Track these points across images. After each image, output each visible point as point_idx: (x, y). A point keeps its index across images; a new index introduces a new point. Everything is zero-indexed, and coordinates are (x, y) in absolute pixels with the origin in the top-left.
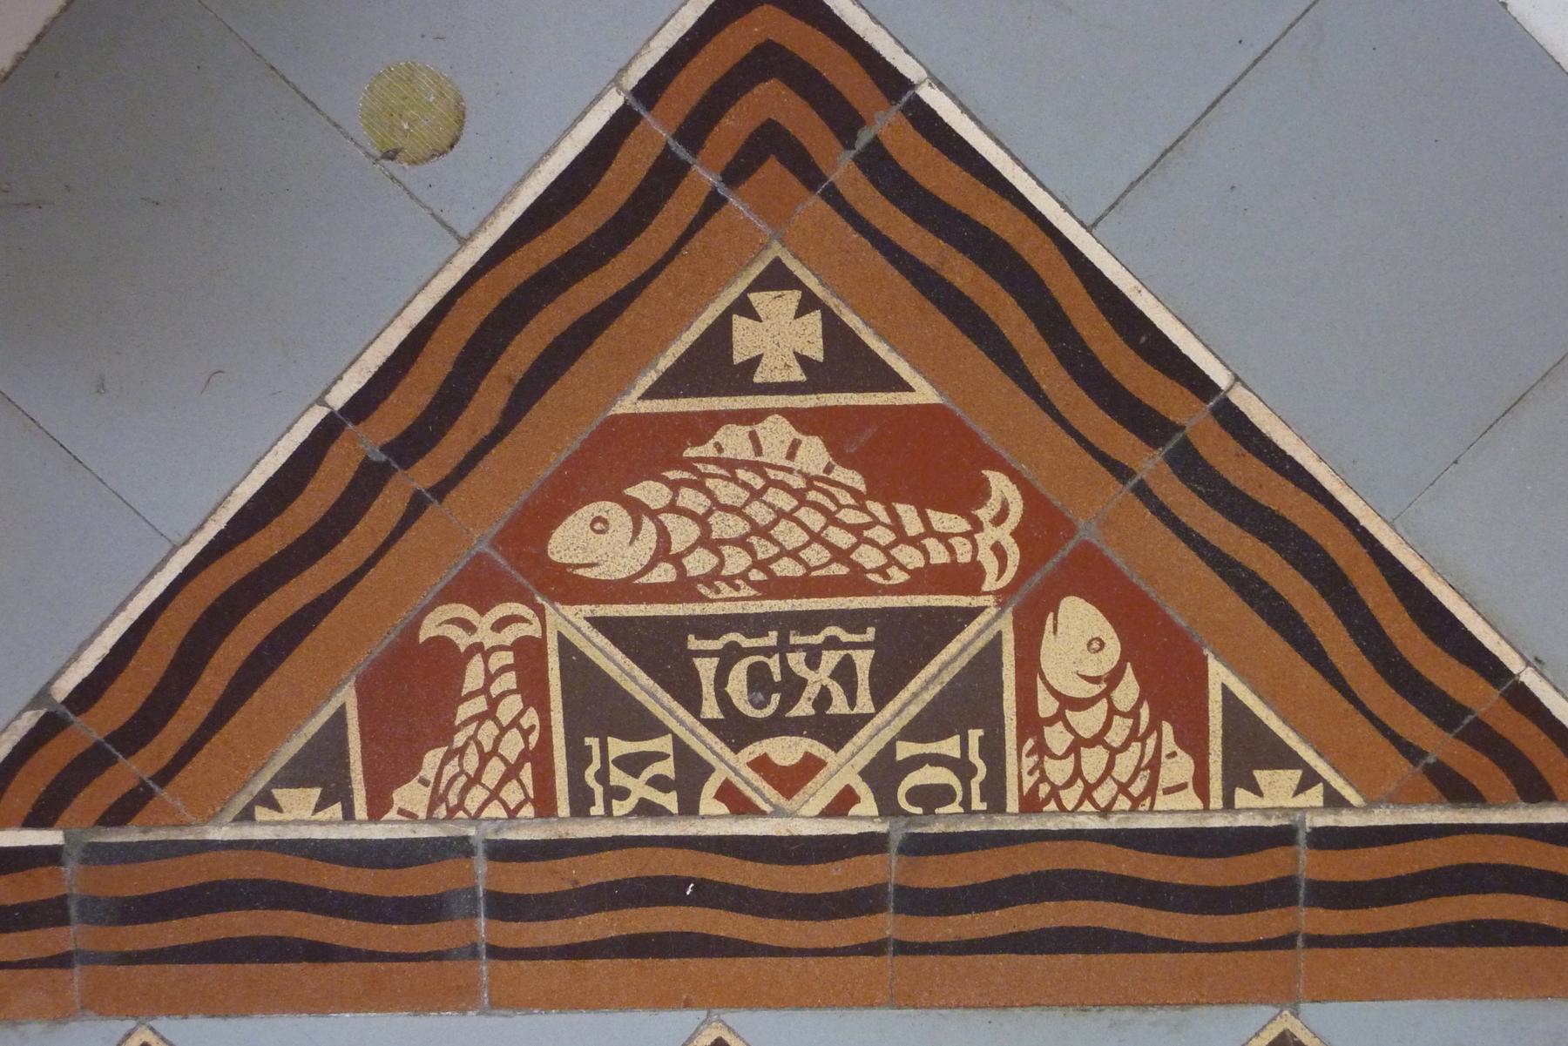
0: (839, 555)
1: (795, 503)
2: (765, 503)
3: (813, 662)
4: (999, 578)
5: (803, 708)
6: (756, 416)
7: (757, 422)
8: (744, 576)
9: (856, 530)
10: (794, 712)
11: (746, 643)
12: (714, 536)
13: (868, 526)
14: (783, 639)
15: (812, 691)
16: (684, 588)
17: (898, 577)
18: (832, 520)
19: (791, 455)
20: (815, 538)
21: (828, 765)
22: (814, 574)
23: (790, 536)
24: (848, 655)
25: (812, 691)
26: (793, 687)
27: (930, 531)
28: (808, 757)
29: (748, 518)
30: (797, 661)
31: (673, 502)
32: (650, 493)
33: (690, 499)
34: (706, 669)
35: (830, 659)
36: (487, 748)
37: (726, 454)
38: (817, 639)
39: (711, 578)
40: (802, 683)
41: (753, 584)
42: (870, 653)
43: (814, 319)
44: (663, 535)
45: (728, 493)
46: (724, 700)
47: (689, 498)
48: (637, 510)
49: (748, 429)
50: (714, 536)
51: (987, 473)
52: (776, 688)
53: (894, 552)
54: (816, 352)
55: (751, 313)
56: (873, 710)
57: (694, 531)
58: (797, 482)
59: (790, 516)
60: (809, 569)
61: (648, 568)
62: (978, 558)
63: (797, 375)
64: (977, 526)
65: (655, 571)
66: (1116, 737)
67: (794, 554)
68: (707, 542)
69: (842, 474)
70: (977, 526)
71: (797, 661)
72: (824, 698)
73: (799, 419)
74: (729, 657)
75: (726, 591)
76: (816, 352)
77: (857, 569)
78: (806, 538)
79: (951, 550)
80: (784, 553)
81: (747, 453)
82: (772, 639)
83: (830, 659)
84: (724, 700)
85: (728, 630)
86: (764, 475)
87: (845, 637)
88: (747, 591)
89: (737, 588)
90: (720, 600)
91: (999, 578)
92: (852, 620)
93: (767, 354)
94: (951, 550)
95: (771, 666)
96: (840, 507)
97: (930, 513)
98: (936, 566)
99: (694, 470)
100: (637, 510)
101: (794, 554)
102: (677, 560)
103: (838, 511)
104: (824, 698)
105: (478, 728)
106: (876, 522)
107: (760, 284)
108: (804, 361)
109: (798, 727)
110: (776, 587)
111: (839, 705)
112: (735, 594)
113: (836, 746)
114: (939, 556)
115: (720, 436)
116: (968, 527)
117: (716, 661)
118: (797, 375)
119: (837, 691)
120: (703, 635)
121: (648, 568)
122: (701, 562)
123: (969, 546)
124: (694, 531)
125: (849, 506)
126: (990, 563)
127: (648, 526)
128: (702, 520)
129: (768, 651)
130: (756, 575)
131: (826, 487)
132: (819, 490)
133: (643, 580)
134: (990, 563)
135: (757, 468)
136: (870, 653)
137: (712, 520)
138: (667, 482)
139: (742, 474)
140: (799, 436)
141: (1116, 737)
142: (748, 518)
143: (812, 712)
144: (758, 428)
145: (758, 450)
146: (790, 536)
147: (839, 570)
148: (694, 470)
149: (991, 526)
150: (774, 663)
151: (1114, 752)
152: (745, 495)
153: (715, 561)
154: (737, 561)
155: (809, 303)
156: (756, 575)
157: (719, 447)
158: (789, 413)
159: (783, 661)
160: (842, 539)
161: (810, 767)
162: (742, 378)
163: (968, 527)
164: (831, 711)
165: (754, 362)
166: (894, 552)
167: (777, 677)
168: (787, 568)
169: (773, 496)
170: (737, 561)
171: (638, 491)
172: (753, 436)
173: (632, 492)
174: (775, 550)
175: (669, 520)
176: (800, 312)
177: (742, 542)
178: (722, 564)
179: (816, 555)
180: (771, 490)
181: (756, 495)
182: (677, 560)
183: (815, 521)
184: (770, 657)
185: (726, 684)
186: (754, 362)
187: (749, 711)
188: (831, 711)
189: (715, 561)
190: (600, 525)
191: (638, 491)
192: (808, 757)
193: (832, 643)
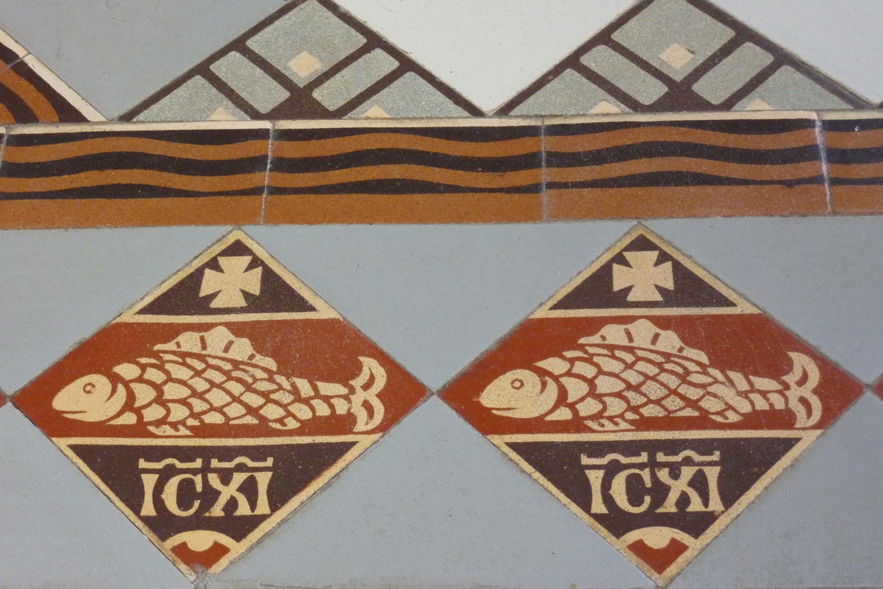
0: (251, 411)
1: (225, 378)
2: (635, 370)
3: (675, 474)
4: (367, 424)
5: (217, 511)
6: (208, 327)
7: (630, 323)
8: (621, 416)
9: (265, 395)
10: (660, 510)
11: (179, 465)
12: (598, 392)
13: (274, 391)
14: (652, 457)
15: (222, 501)
16: (577, 424)
17: (292, 424)
18: (249, 388)
19: (226, 350)
20: (236, 399)
21: (231, 551)
22: (232, 422)
23: (218, 398)
24: (252, 475)
25: (222, 501)
26: (211, 494)
27: (753, 389)
28: (673, 541)
29: (190, 387)
30: (214, 480)
31: (570, 370)
32: (127, 370)
33: (155, 375)
34: (595, 478)
35: (688, 472)
36: (711, 389)
37: (609, 341)
38: (678, 458)
39: (159, 423)
40: (668, 489)
41: (191, 428)
42: (717, 469)
43: (668, 265)
44: (131, 397)
45: (182, 373)
46: (608, 500)
47: (581, 368)
48: (115, 379)
49: (624, 327)
50: (598, 392)
51: (138, 360)
52: (197, 496)
53: (289, 408)
54: (670, 285)
55: (625, 263)
56: (268, 512)
57: (152, 394)
58: (228, 367)
59: (654, 378)
60: (228, 419)
61: (552, 411)
62: (789, 406)
63: (658, 297)
64: (352, 390)
65: (558, 411)
66: (589, 371)
67: (658, 402)
68: (593, 393)
69: (259, 360)
70: (787, 387)
71: (214, 480)
72: (232, 504)
73: (658, 321)
74: (612, 470)
75: (609, 426)
76: (670, 285)
77: (263, 420)
78: (229, 399)
79: (331, 406)
80: (212, 408)
81: (197, 349)
82: (198, 463)
83: (239, 478)
84: (608, 500)
85: (165, 456)
86: (634, 354)
87: (697, 458)
88: (623, 425)
89: (617, 424)
90: (604, 432)
91: (367, 424)
92: (704, 446)
93: (653, 282)
94: (331, 406)
95: (196, 481)
96: (255, 380)
97: (751, 377)
98: (321, 417)
99: (586, 352)
100: (115, 379)
101: (220, 410)
102: (138, 412)
103: (253, 383)
104: (684, 500)
105: (289, 392)
106: (280, 388)
107: (225, 253)
108: (661, 290)
109: (667, 520)
110: (198, 432)
111: (696, 505)
112: (616, 428)
113: (696, 534)
114: (323, 410)
115: (181, 338)
116: (780, 387)
117: (157, 476)
118: (658, 297)
119: (242, 500)
120: (148, 459)
121: (552, 411)
122: (588, 408)
123: (782, 400)
124: (152, 394)
125: (696, 372)
126: (361, 414)
127: (552, 387)
128: (158, 388)
129: (195, 472)
130: (191, 422)
131: (680, 361)
132: (675, 363)
133: (113, 422)
134: (361, 414)
135: (630, 350)
136: (717, 469)
137: (597, 381)
138: (138, 364)
139: (618, 353)
140: (659, 331)
141: (589, 371)
142: (190, 387)
143: (222, 514)
144: (206, 335)
145: (631, 340)
146: (218, 398)
147: (250, 420)
148: (586, 352)
149: (361, 391)
150: (198, 480)
151: (601, 372)
152: (622, 366)
153: (601, 407)
154: (179, 413)
155: (664, 257)
156: (630, 416)
157: (603, 338)
158: (228, 325)
159: (653, 476)
160: (254, 400)
161: (218, 551)
162: (203, 306)
163: (780, 387)
164: (238, 513)
165: (628, 290)
166: (290, 408)
167: (648, 484)
168: (650, 411)
169: (641, 366)
170: (179, 413)
171: (544, 364)
172: (202, 339)
173: (540, 364)
174: (644, 400)
175: (136, 387)
176: (626, 264)
177: (184, 402)
178: (605, 408)
179: (234, 410)
180: (641, 363)
181: (629, 366)
182: (572, 406)
183: (236, 388)
184: (195, 475)
185: (610, 488)
186: (628, 290)
187: (184, 514)
188: (238, 513)
189: (601, 407)
190: (88, 390)
191: (544, 364)
192: (673, 541)
193: (688, 461)
